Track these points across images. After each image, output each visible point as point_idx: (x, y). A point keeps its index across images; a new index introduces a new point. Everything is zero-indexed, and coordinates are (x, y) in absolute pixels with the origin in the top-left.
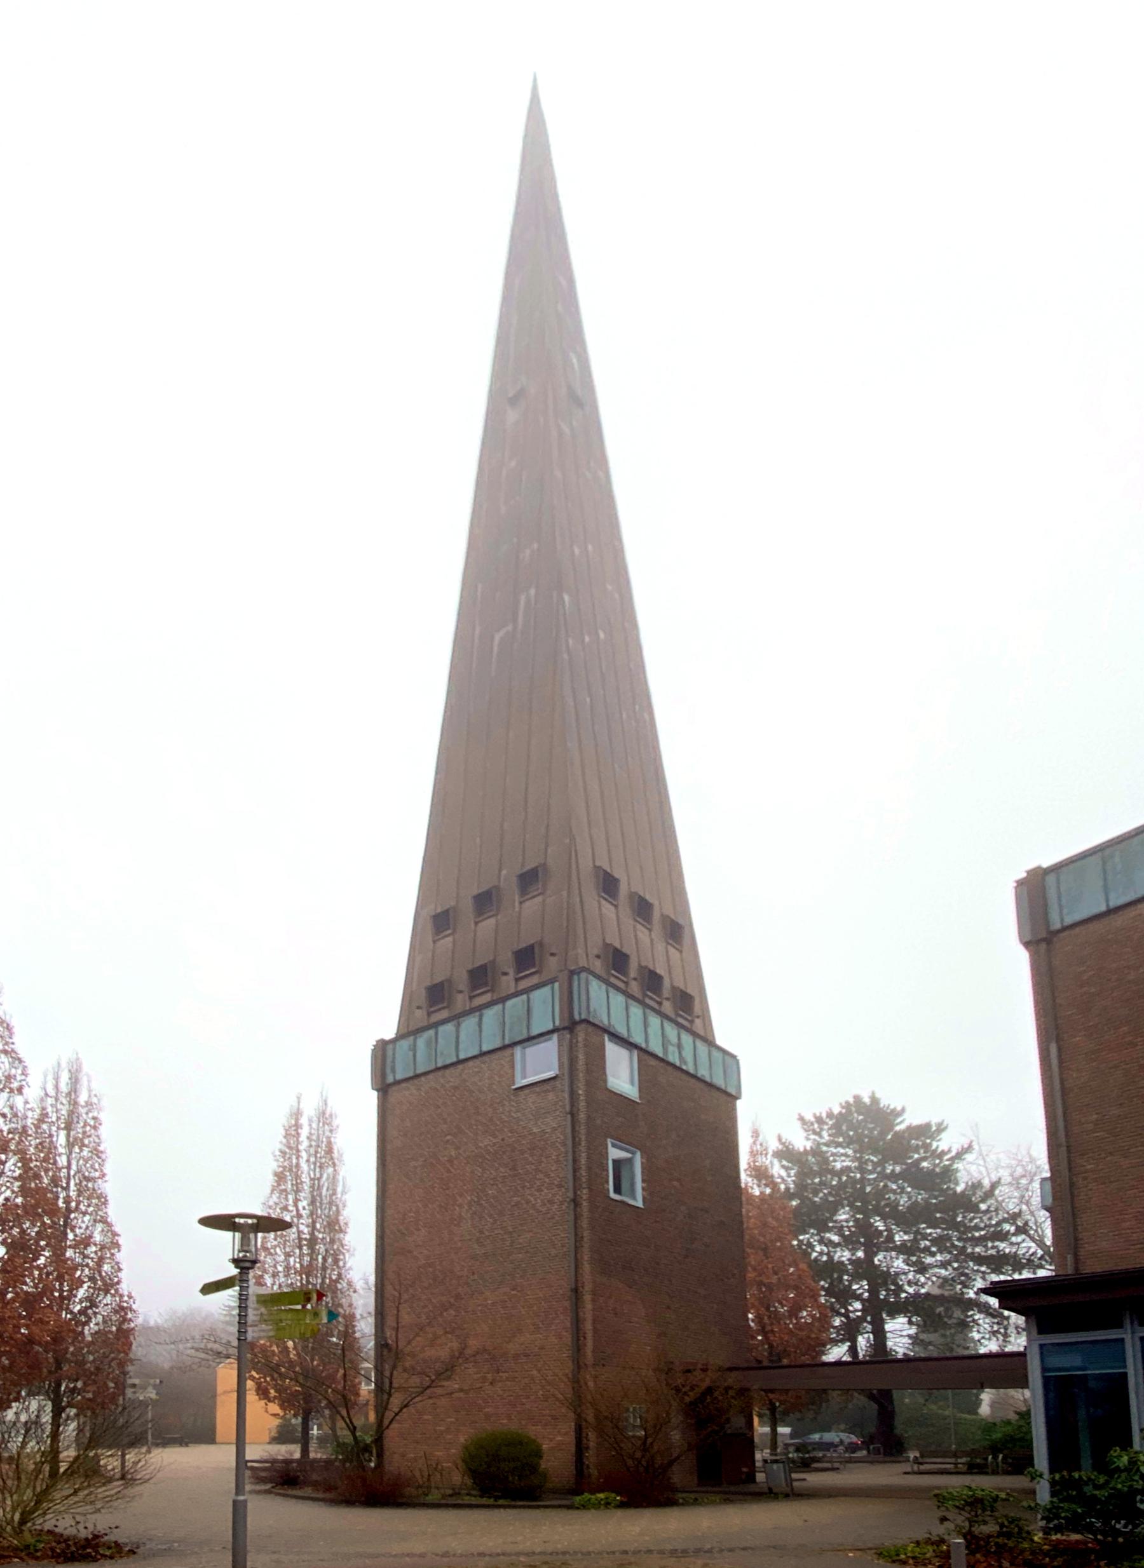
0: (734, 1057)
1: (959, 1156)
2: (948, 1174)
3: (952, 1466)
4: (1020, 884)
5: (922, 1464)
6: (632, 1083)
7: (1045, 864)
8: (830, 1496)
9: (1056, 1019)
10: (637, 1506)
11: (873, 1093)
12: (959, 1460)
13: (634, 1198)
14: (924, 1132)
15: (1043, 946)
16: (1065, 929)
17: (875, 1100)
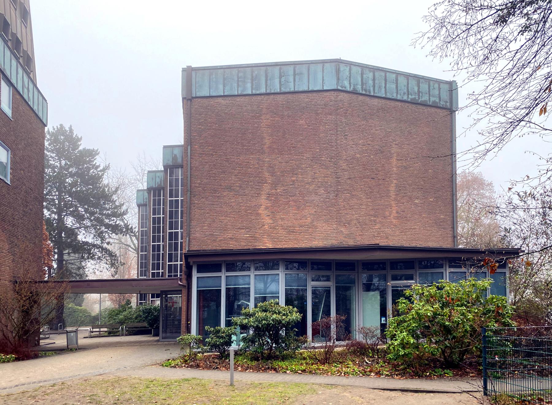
0: (46, 101)
1: (104, 170)
2: (98, 178)
3: (98, 333)
4: (184, 70)
5: (92, 332)
6: (9, 108)
7: (194, 66)
8: (94, 348)
9: (191, 135)
10: (23, 360)
11: (71, 126)
12: (102, 330)
13: (6, 176)
14: (92, 154)
15: (189, 101)
16: (196, 97)
17: (71, 130)
